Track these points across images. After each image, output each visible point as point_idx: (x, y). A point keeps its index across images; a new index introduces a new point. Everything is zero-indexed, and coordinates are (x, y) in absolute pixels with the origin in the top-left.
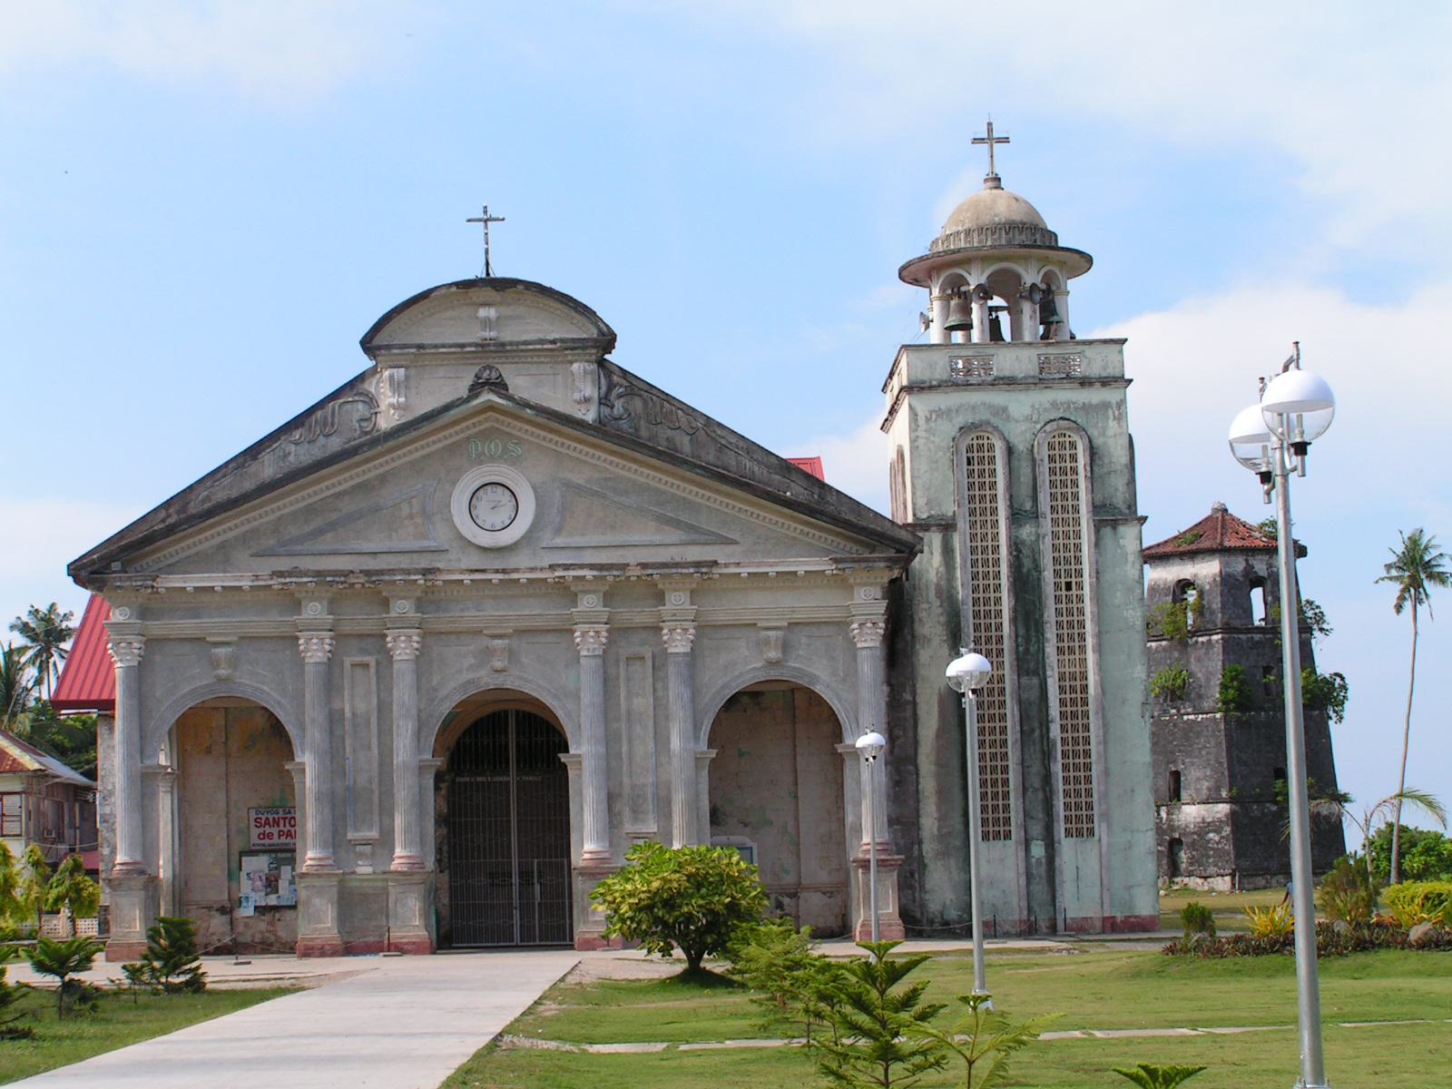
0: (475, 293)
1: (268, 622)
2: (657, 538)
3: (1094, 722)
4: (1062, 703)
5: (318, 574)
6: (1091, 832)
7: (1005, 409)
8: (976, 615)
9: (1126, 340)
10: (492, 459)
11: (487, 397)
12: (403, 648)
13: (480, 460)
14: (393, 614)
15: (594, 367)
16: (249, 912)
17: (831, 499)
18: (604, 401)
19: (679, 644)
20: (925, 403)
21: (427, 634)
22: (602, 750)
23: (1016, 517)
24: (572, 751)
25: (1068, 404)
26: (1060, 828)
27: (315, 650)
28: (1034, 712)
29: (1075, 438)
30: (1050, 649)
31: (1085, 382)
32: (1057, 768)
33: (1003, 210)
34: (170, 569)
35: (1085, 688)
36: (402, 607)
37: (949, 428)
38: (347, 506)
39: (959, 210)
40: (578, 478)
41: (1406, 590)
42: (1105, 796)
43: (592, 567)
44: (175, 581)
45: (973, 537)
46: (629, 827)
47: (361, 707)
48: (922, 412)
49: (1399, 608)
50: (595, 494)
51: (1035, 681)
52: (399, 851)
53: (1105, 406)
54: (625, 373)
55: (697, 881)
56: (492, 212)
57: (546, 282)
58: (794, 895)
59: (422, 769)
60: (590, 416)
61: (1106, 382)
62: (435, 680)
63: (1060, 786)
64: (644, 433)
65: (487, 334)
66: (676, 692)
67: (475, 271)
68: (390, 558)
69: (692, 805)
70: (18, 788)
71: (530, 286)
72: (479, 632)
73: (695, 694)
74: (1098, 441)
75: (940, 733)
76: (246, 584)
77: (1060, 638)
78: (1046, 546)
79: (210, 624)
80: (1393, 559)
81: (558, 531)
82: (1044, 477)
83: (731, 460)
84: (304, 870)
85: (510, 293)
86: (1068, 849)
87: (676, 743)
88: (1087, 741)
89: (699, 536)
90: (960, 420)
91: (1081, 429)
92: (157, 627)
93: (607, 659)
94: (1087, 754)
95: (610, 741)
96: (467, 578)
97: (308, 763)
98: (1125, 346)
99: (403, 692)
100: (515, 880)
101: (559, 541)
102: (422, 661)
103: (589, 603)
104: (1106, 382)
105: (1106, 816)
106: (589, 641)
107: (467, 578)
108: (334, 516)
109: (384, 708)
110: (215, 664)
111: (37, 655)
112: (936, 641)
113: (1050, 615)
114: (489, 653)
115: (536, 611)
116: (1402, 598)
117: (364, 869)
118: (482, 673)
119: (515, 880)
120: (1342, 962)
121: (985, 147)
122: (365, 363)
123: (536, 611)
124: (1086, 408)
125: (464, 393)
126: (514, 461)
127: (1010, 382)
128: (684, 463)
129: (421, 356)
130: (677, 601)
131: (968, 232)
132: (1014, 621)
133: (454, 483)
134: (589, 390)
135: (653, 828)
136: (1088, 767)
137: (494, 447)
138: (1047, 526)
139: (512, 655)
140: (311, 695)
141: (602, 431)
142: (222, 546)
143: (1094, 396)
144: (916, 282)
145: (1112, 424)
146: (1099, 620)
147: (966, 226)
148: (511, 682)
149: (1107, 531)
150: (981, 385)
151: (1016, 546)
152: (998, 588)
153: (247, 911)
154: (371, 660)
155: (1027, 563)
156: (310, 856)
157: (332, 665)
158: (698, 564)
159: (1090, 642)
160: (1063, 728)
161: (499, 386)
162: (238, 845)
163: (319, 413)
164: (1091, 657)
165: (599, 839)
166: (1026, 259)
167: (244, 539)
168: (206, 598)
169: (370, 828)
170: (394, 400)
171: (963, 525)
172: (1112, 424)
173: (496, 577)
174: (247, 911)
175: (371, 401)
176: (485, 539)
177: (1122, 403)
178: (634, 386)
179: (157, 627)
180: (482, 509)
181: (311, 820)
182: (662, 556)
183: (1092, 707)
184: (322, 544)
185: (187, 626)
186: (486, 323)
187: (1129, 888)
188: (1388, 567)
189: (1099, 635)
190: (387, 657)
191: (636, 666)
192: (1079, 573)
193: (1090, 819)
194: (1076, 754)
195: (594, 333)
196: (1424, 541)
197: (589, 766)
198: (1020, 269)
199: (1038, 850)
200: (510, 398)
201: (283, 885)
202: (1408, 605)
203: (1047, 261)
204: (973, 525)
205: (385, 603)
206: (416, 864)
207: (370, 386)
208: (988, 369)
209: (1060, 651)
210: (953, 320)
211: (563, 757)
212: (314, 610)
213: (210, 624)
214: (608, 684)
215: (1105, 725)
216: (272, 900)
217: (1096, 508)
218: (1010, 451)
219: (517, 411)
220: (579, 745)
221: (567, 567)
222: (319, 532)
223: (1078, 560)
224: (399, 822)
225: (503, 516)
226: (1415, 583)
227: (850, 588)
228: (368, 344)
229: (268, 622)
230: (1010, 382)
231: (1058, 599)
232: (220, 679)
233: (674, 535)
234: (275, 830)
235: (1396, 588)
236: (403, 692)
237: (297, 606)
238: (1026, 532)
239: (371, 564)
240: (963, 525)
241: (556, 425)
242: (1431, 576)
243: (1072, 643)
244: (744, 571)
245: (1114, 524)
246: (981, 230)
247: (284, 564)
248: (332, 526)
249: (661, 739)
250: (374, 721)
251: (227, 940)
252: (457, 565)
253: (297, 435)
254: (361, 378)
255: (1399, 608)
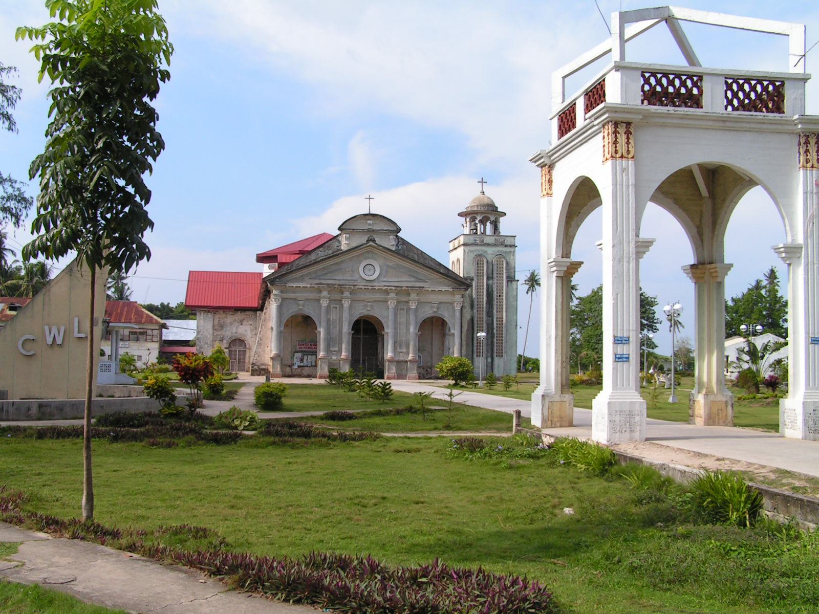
0: (367, 217)
1: (312, 296)
2: (409, 280)
3: (504, 329)
4: (497, 324)
5: (328, 284)
6: (502, 356)
7: (486, 251)
8: (478, 302)
9: (582, 263)
10: (370, 258)
11: (371, 243)
12: (346, 304)
13: (366, 258)
14: (344, 295)
15: (395, 237)
16: (296, 367)
17: (450, 272)
18: (397, 245)
19: (413, 307)
20: (467, 249)
21: (353, 301)
22: (393, 331)
23: (488, 278)
24: (386, 331)
25: (501, 251)
26: (495, 355)
27: (324, 303)
28: (490, 326)
29: (503, 260)
30: (495, 311)
31: (506, 246)
32: (495, 340)
33: (486, 201)
34: (290, 281)
35: (502, 321)
36: (347, 294)
37: (473, 255)
38: (333, 268)
39: (475, 199)
40: (390, 264)
41: (530, 288)
42: (506, 347)
43: (394, 286)
44: (291, 285)
45: (478, 283)
46: (399, 350)
47: (334, 318)
48: (467, 251)
49: (527, 293)
50: (395, 269)
51: (491, 318)
52: (343, 354)
53: (510, 252)
54: (402, 239)
55: (460, 365)
56: (371, 197)
57: (385, 216)
58: (430, 368)
59: (349, 333)
60: (394, 249)
61: (511, 246)
62: (353, 312)
63: (495, 345)
64: (406, 254)
65: (370, 227)
66: (412, 318)
67: (367, 212)
68: (344, 281)
69: (415, 346)
70: (158, 328)
71: (381, 216)
72: (363, 301)
73: (416, 318)
74: (508, 261)
75: (468, 330)
76: (309, 286)
77: (497, 308)
78: (495, 286)
79: (299, 296)
80: (526, 278)
81: (385, 277)
82: (495, 267)
83: (427, 261)
84: (320, 357)
85: (376, 217)
86: (496, 359)
87: (411, 330)
88: (502, 334)
89: (419, 280)
90: (476, 253)
91: (504, 258)
92: (285, 295)
93: (396, 309)
94: (502, 337)
95: (395, 329)
96: (363, 287)
97: (322, 331)
98: (516, 238)
99: (346, 315)
100: (361, 361)
101: (385, 279)
102: (350, 307)
103: (392, 295)
104: (511, 246)
105: (506, 352)
106: (391, 304)
107: (363, 287)
108: (330, 270)
109: (341, 318)
110: (299, 305)
111: (115, 284)
112: (467, 308)
113: (495, 303)
114: (366, 306)
115: (378, 296)
116: (528, 290)
117: (334, 358)
118: (364, 311)
119: (361, 361)
120: (594, 387)
121: (481, 184)
122: (339, 232)
123: (378, 296)
124: (506, 252)
125: (365, 242)
126: (375, 259)
127: (488, 245)
128: (415, 261)
129: (353, 232)
130: (413, 296)
131: (477, 206)
132: (486, 303)
133: (360, 264)
134: (394, 243)
135: (405, 351)
136: (502, 340)
137: (371, 255)
138: (495, 281)
139: (372, 307)
140: (323, 315)
141: (396, 253)
142: (301, 276)
143: (508, 249)
144: (461, 216)
145: (512, 256)
146: (507, 305)
147: (477, 204)
148: (371, 313)
149: (509, 283)
150: (481, 245)
151: (488, 285)
152: (483, 295)
153: (296, 367)
154: (338, 306)
155: (490, 290)
156: (321, 354)
157: (328, 307)
158: (420, 287)
159: (504, 310)
160: (497, 331)
161: (374, 241)
162: (294, 350)
163: (327, 244)
164: (504, 314)
165: (392, 353)
166: (492, 214)
167: (307, 274)
168: (298, 289)
169: (336, 347)
170: (346, 242)
171: (475, 279)
172: (512, 256)
173: (370, 288)
174: (296, 367)
175: (339, 242)
176: (367, 278)
177: (514, 252)
178: (404, 242)
179: (285, 295)
180: (366, 270)
181: (322, 345)
182: (410, 284)
183: (504, 325)
184: (328, 276)
185: (292, 295)
186: (370, 225)
187: (510, 370)
188: (526, 281)
189: (506, 308)
190: (342, 305)
191: (402, 311)
192: (503, 293)
193: (502, 353)
194: (499, 337)
195: (395, 228)
196: (535, 274)
197: (390, 335)
198: (490, 216)
199: (489, 360)
200: (376, 244)
201: (305, 360)
202: (530, 292)
203: (496, 214)
204: (478, 279)
205: (342, 293)
206: (348, 357)
207: (340, 238)
208: (483, 241)
209: (497, 311)
210: (473, 227)
211: (383, 333)
212: (325, 293)
213: (299, 296)
214: (396, 315)
215: (507, 330)
216: (302, 364)
217: (508, 277)
218: (487, 262)
219: (378, 247)
220: (388, 329)
221: (388, 286)
222: (326, 274)
223: (502, 290)
224: (344, 346)
225: (370, 273)
226: (533, 286)
227: (454, 295)
228: (340, 229)
229: (312, 296)
230: (488, 245)
231: (497, 299)
232: (434, 312)
233: (413, 279)
234: (303, 347)
235: (527, 286)
236: (346, 315)
237: (320, 292)
238: (490, 282)
239: (340, 283)
240: (475, 279)
241: (387, 251)
242: (537, 284)
243: (500, 310)
244: (430, 289)
245: (511, 281)
246: (481, 205)
247: (317, 281)
248: (329, 272)
249: (408, 329)
250: (338, 321)
251: (290, 374)
252: (361, 285)
253: (321, 249)
254: (337, 236)
255: (527, 293)
